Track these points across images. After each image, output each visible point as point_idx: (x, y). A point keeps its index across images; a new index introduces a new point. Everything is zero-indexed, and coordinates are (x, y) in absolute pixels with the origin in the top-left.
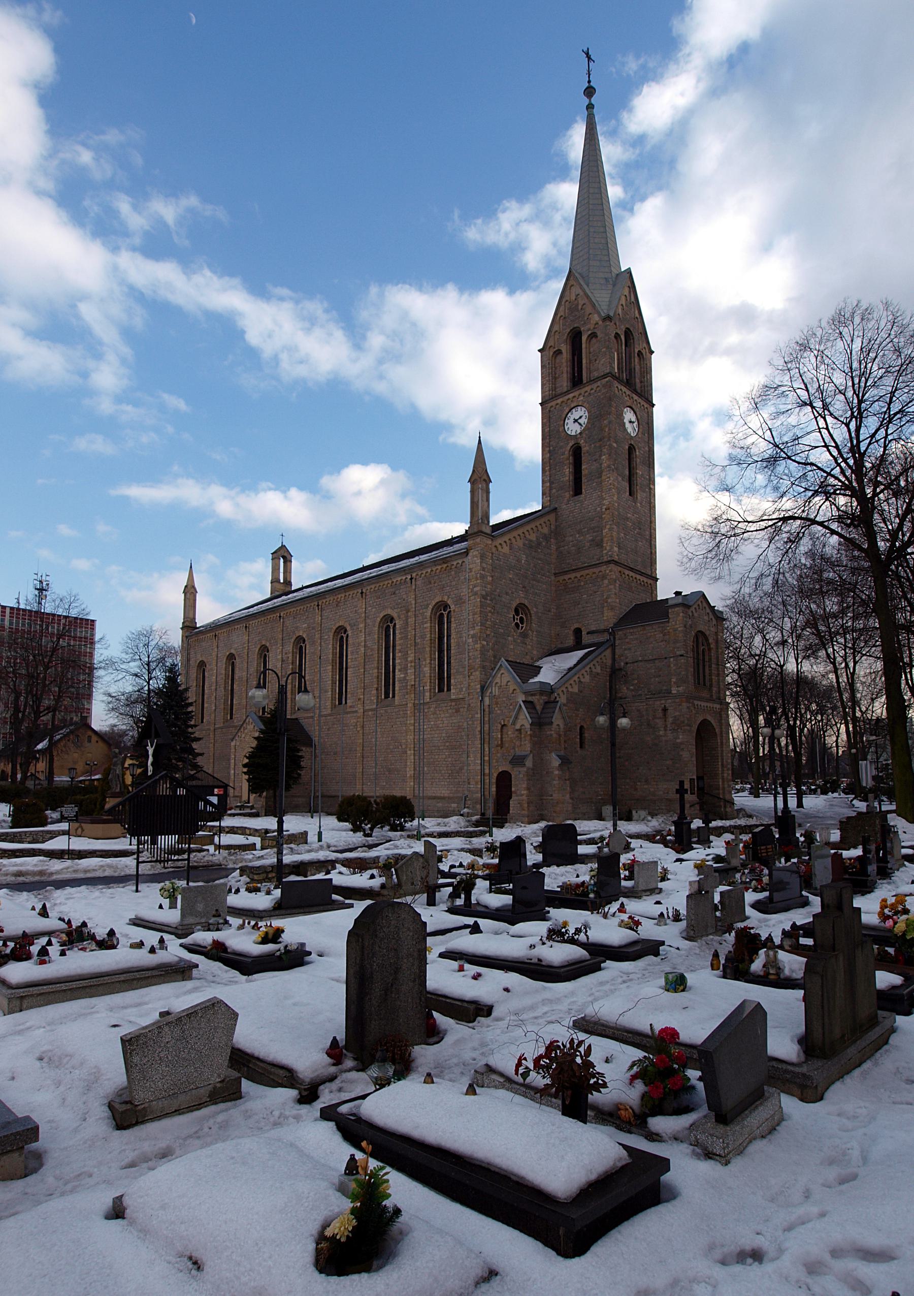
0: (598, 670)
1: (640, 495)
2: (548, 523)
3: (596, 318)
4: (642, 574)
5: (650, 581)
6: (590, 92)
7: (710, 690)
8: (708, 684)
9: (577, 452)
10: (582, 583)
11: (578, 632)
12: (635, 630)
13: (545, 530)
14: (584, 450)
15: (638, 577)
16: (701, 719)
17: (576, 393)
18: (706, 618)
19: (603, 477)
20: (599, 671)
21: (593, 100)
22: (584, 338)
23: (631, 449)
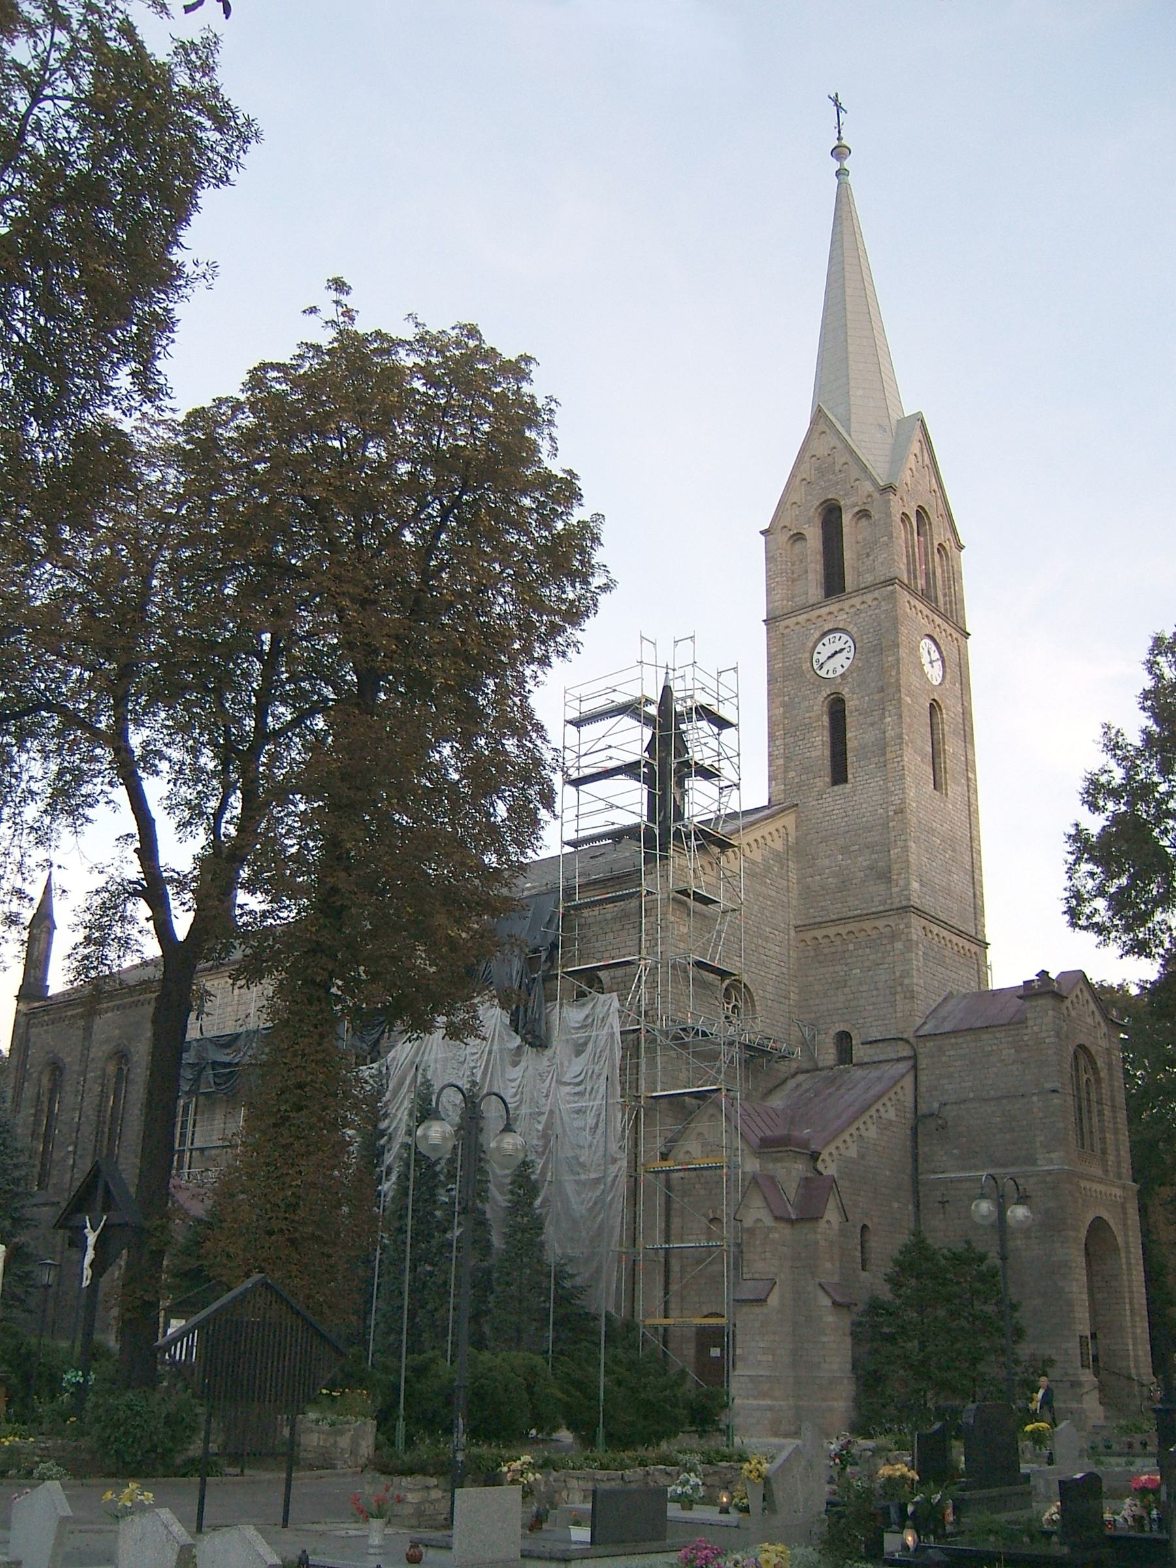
0: (891, 1114)
1: (954, 790)
2: (782, 830)
3: (868, 487)
4: (960, 933)
5: (974, 948)
6: (840, 152)
7: (1104, 1162)
8: (1098, 1147)
9: (837, 710)
10: (851, 947)
11: (844, 1039)
12: (960, 1040)
13: (778, 845)
14: (850, 705)
15: (955, 939)
16: (1090, 1217)
17: (834, 608)
18: (1090, 1020)
19: (889, 756)
20: (894, 1118)
21: (847, 164)
22: (847, 518)
23: (934, 707)
